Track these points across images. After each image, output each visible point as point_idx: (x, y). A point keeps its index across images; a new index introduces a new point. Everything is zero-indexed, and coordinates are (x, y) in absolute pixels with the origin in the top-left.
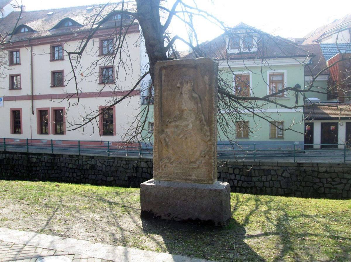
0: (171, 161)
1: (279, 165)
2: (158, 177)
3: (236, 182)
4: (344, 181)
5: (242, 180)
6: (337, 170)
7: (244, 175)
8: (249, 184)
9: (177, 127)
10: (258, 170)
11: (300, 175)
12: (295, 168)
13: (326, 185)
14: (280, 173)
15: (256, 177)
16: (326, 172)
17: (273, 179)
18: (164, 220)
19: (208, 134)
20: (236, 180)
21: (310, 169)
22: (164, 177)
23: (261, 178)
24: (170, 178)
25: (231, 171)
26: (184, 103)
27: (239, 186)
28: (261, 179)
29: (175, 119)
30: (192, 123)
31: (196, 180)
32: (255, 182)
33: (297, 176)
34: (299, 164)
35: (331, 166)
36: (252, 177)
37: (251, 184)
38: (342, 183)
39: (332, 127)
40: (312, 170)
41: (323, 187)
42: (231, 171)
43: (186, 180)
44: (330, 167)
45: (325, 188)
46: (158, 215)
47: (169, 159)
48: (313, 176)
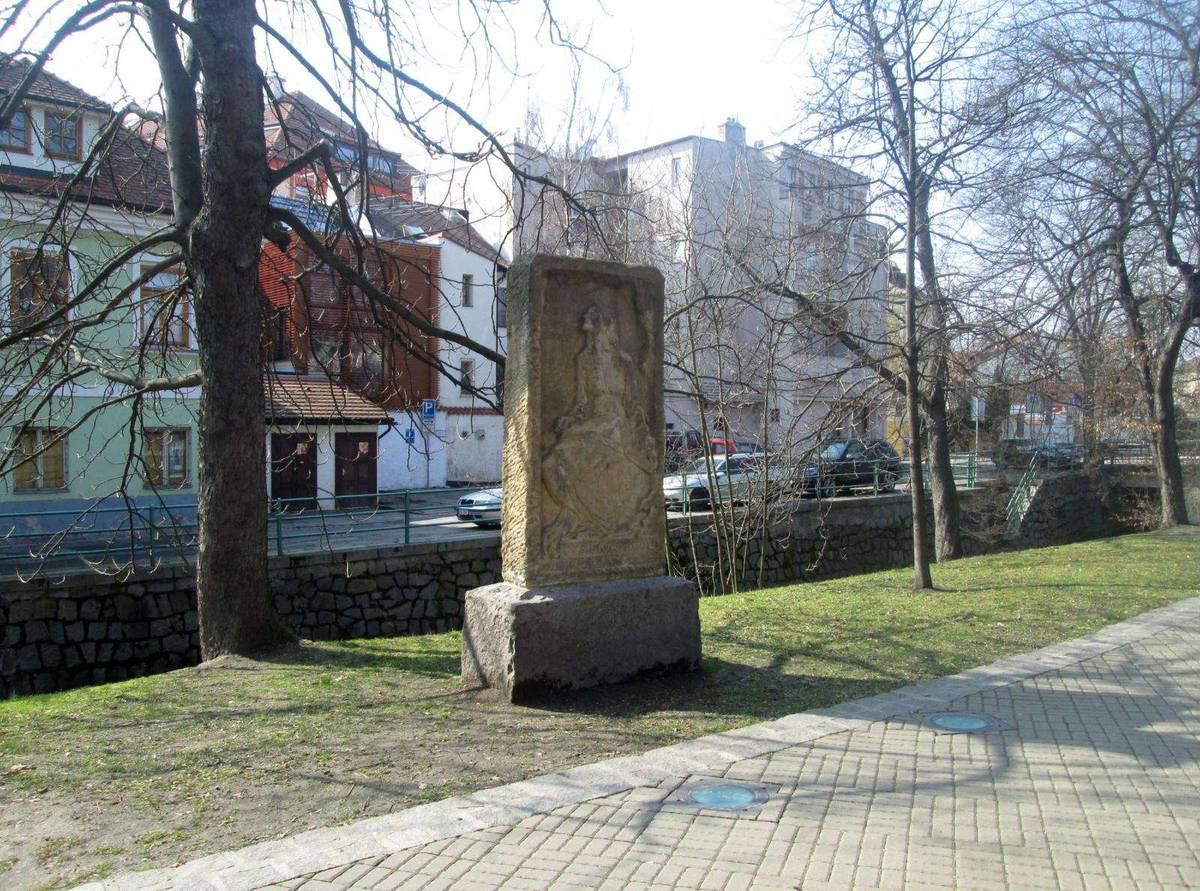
0: (572, 530)
2: (539, 578)
3: (89, 649)
4: (411, 594)
5: (113, 637)
6: (394, 564)
7: (118, 620)
8: (139, 647)
9: (586, 436)
10: (168, 593)
11: (300, 595)
12: (283, 574)
13: (369, 613)
15: (164, 618)
16: (367, 575)
18: (585, 690)
19: (654, 453)
20: (92, 640)
21: (326, 571)
22: (557, 577)
23: (182, 619)
24: (572, 575)
25: (67, 611)
26: (601, 374)
27: (104, 660)
28: (180, 624)
30: (621, 428)
31: (631, 571)
32: (160, 639)
33: (291, 598)
34: (297, 561)
35: (378, 555)
36: (149, 621)
37: (147, 645)
38: (406, 601)
39: (363, 447)
40: (330, 575)
41: (363, 618)
42: (67, 611)
43: (610, 573)
44: (375, 560)
45: (367, 622)
46: (565, 681)
47: (567, 523)
48: (335, 593)
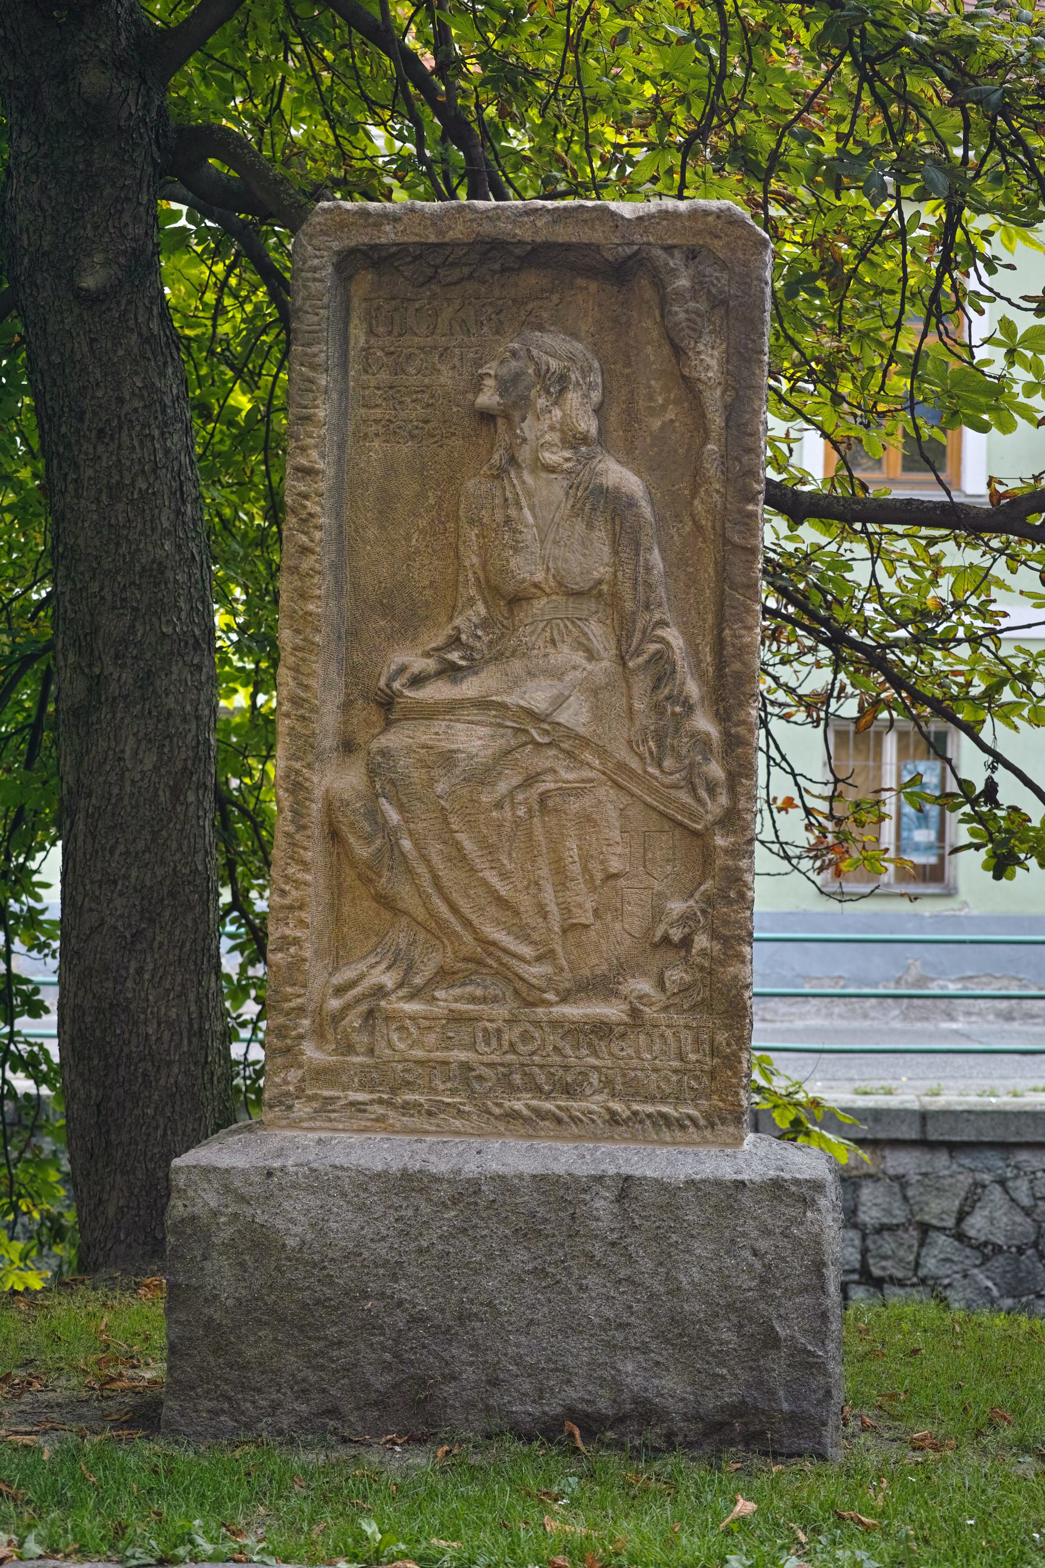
1: (933, 1136)
14: (939, 1209)
17: (876, 1272)
19: (716, 770)
26: (529, 535)
29: (455, 656)
